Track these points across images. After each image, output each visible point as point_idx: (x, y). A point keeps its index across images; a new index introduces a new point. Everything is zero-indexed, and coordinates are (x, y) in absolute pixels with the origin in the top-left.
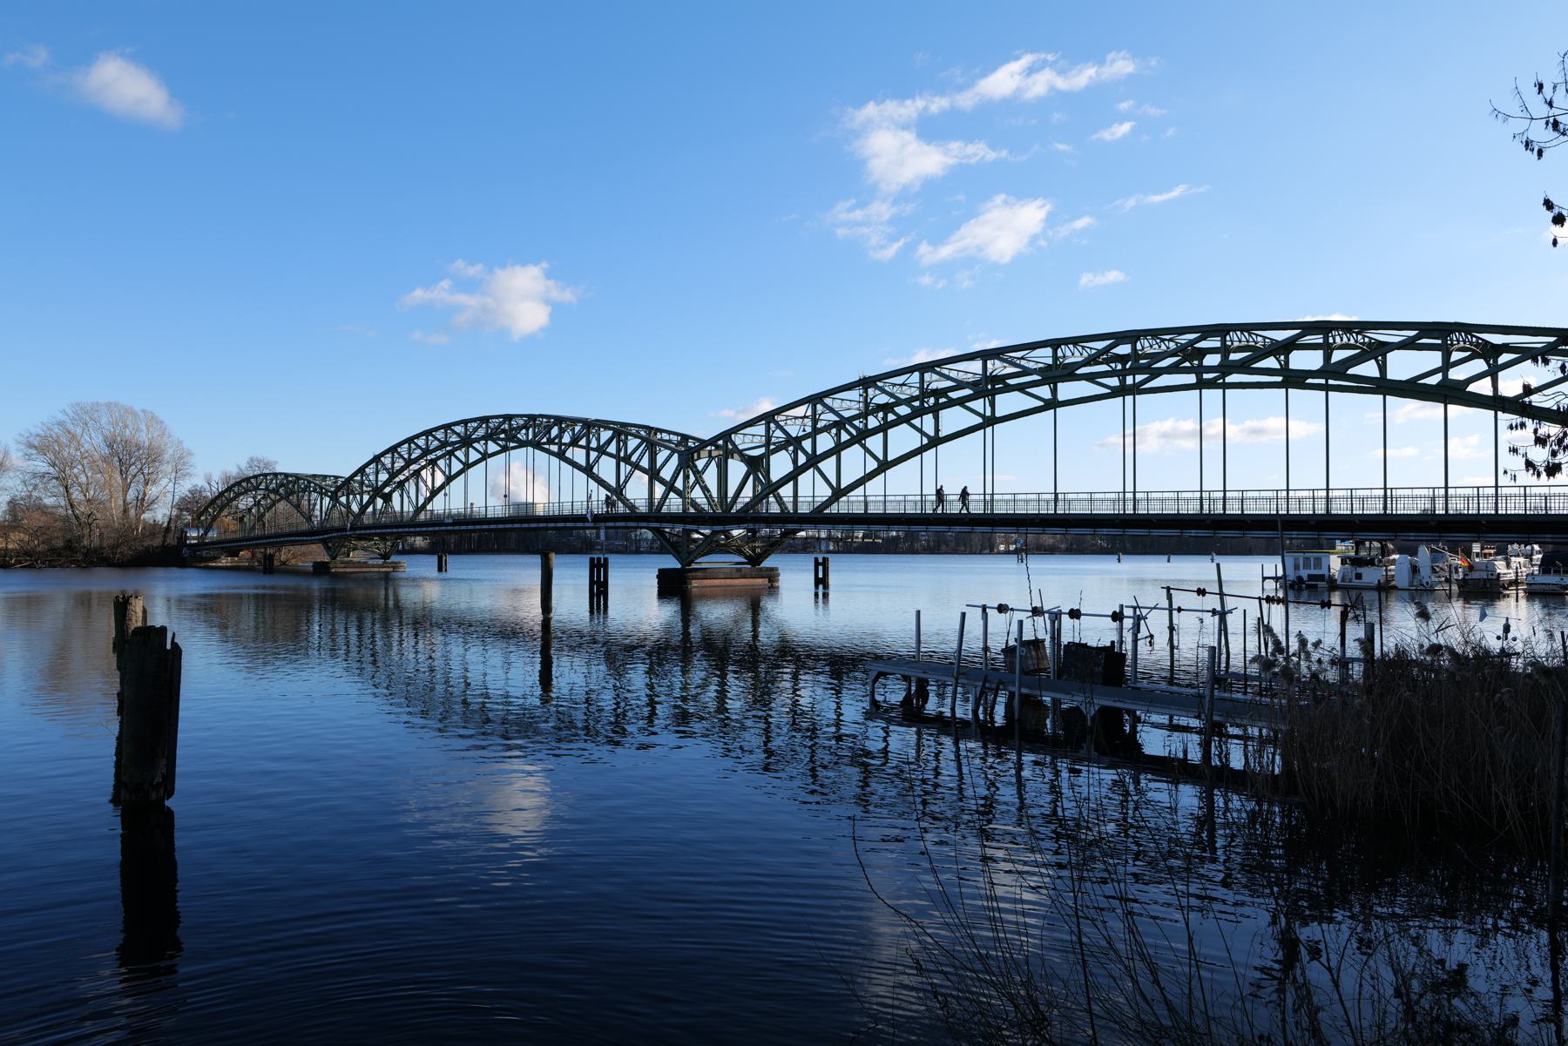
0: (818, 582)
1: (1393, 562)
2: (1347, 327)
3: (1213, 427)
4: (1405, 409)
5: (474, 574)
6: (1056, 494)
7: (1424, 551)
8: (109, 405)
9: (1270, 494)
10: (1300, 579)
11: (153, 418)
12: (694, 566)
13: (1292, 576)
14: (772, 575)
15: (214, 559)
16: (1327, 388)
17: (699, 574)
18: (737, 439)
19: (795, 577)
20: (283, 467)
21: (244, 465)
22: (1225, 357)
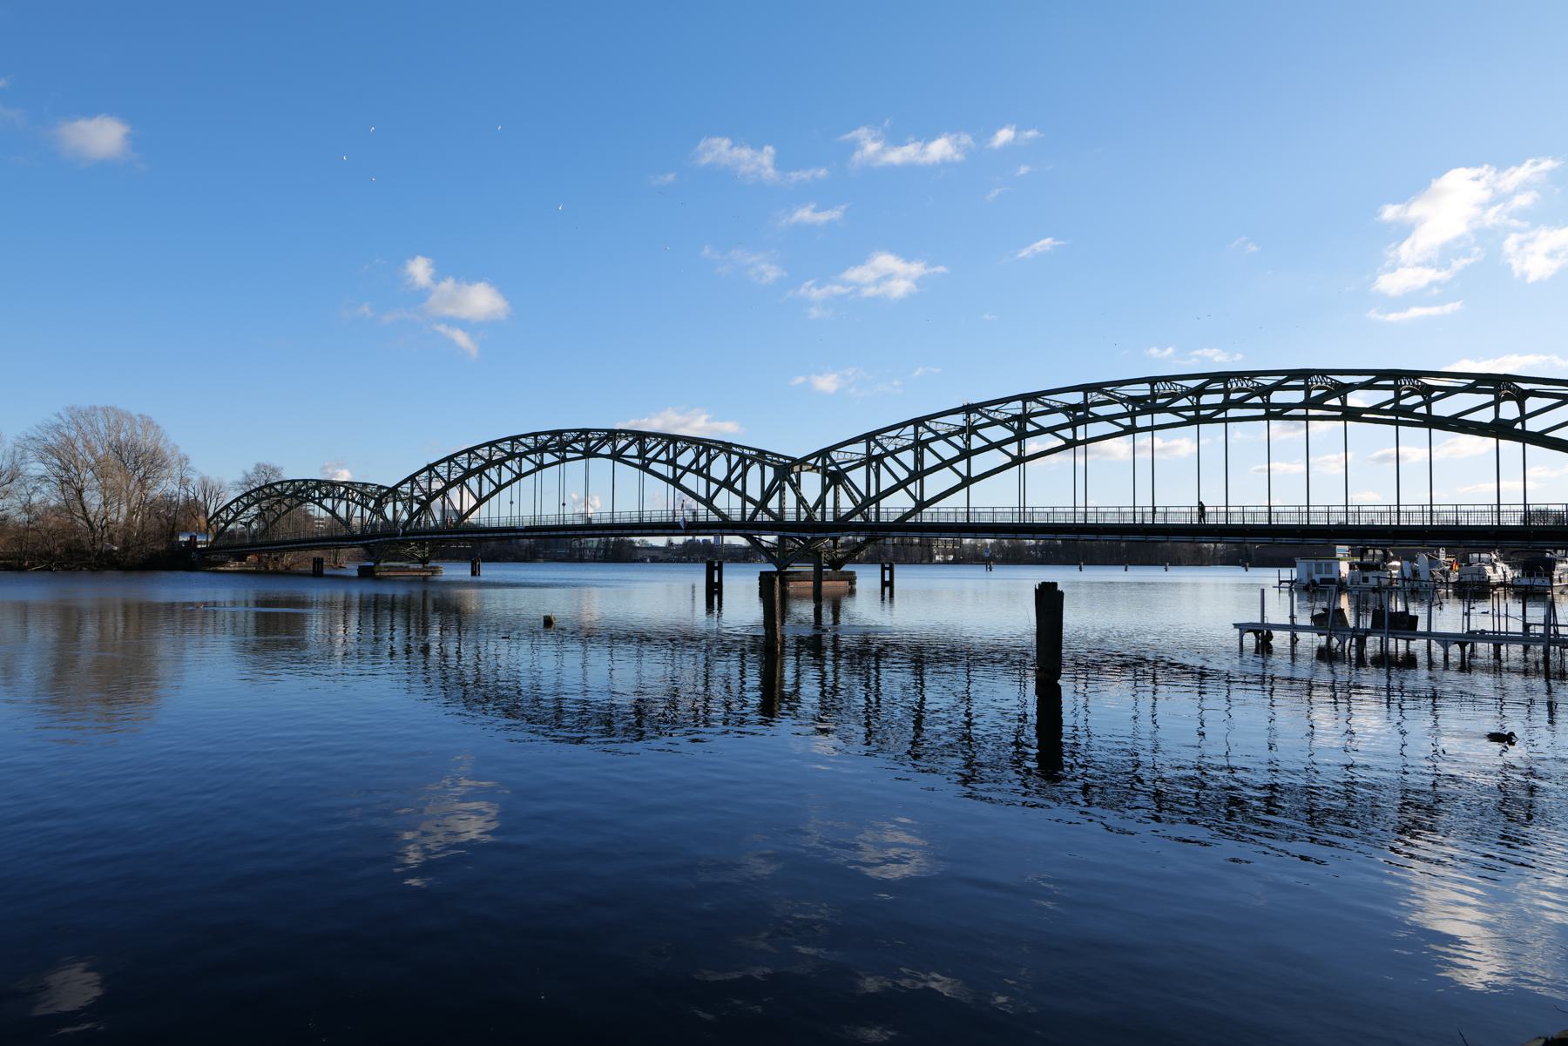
0: (884, 584)
1: (1395, 568)
2: (1240, 375)
3: (1144, 457)
4: (1448, 441)
5: (627, 575)
7: (1423, 558)
8: (105, 410)
10: (1313, 582)
11: (150, 422)
13: (1305, 581)
14: (851, 578)
15: (223, 563)
16: (1397, 423)
18: (834, 455)
19: (867, 578)
20: (288, 474)
21: (250, 470)
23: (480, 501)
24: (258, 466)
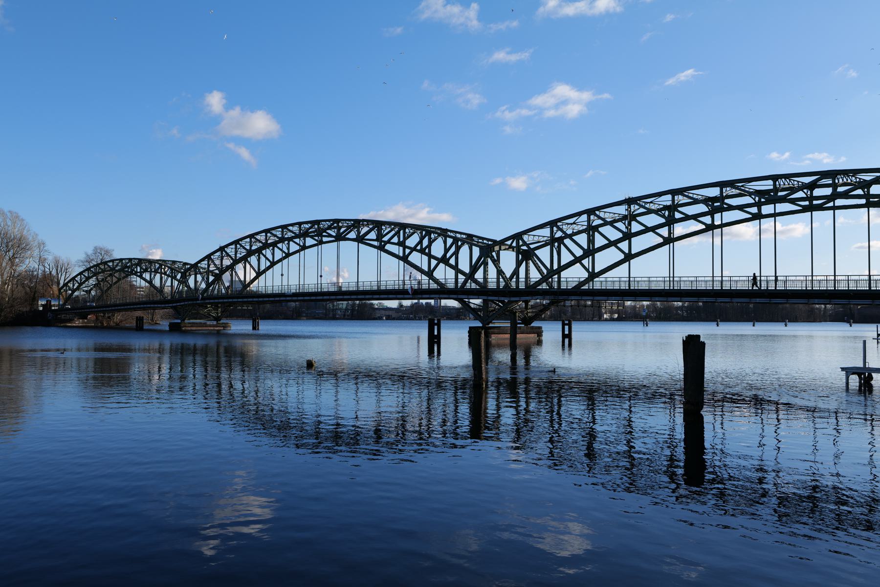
0: (564, 336)
2: (846, 173)
6: (776, 277)
9: (802, 278)
12: (491, 325)
14: (539, 332)
15: (70, 321)
17: (496, 330)
18: (525, 237)
19: (551, 332)
20: (117, 255)
21: (90, 251)
22: (835, 189)
23: (259, 274)
24: (96, 248)
